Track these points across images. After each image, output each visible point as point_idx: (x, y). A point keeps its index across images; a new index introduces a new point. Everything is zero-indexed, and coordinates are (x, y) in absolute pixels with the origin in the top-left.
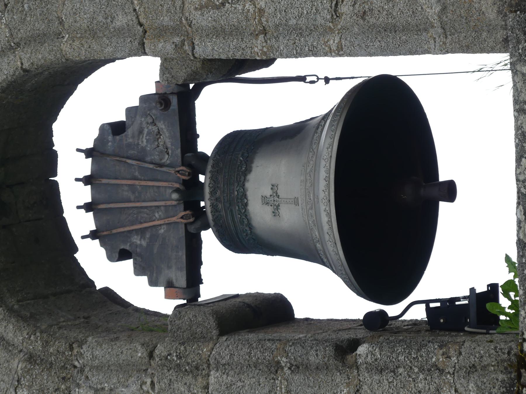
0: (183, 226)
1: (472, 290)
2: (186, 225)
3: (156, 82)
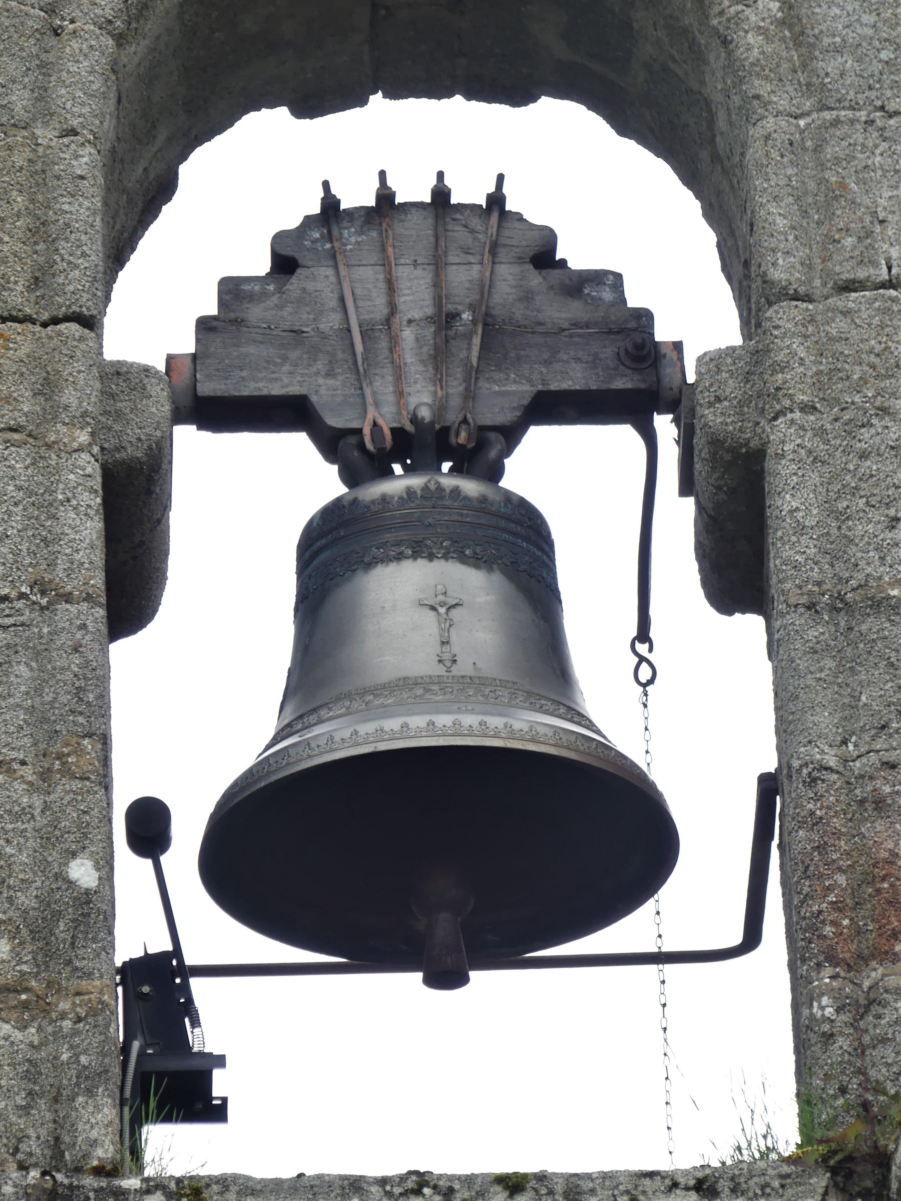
0: (355, 425)
1: (220, 1061)
2: (359, 431)
3: (168, 355)
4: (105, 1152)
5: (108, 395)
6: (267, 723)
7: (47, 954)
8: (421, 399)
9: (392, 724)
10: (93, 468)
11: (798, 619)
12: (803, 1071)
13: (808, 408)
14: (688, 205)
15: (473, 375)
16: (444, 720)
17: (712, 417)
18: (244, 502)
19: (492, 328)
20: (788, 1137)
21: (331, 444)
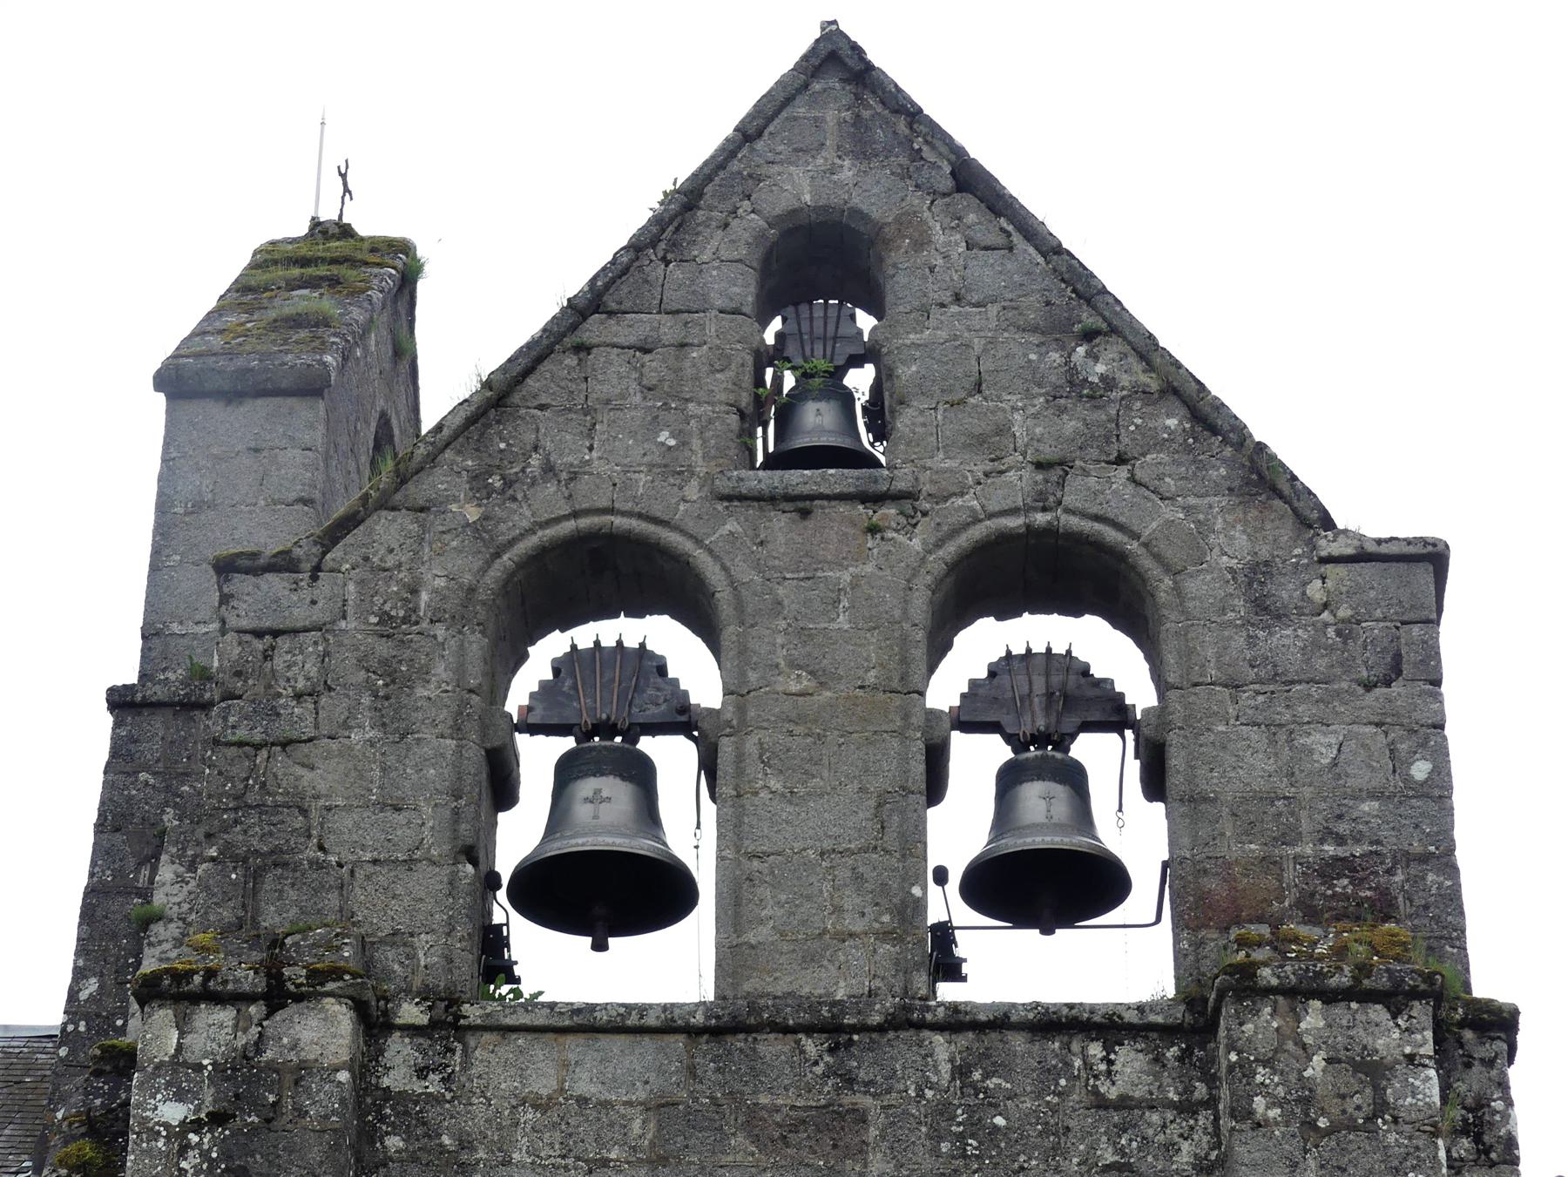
4: (923, 992)
5: (928, 720)
6: (985, 839)
7: (903, 920)
8: (1041, 723)
9: (1029, 840)
10: (922, 746)
11: (1176, 805)
12: (1177, 967)
13: (1181, 728)
14: (1138, 655)
15: (1060, 715)
16: (1048, 839)
17: (1146, 731)
18: (977, 760)
19: (1066, 697)
20: (1171, 992)
21: (1009, 739)
